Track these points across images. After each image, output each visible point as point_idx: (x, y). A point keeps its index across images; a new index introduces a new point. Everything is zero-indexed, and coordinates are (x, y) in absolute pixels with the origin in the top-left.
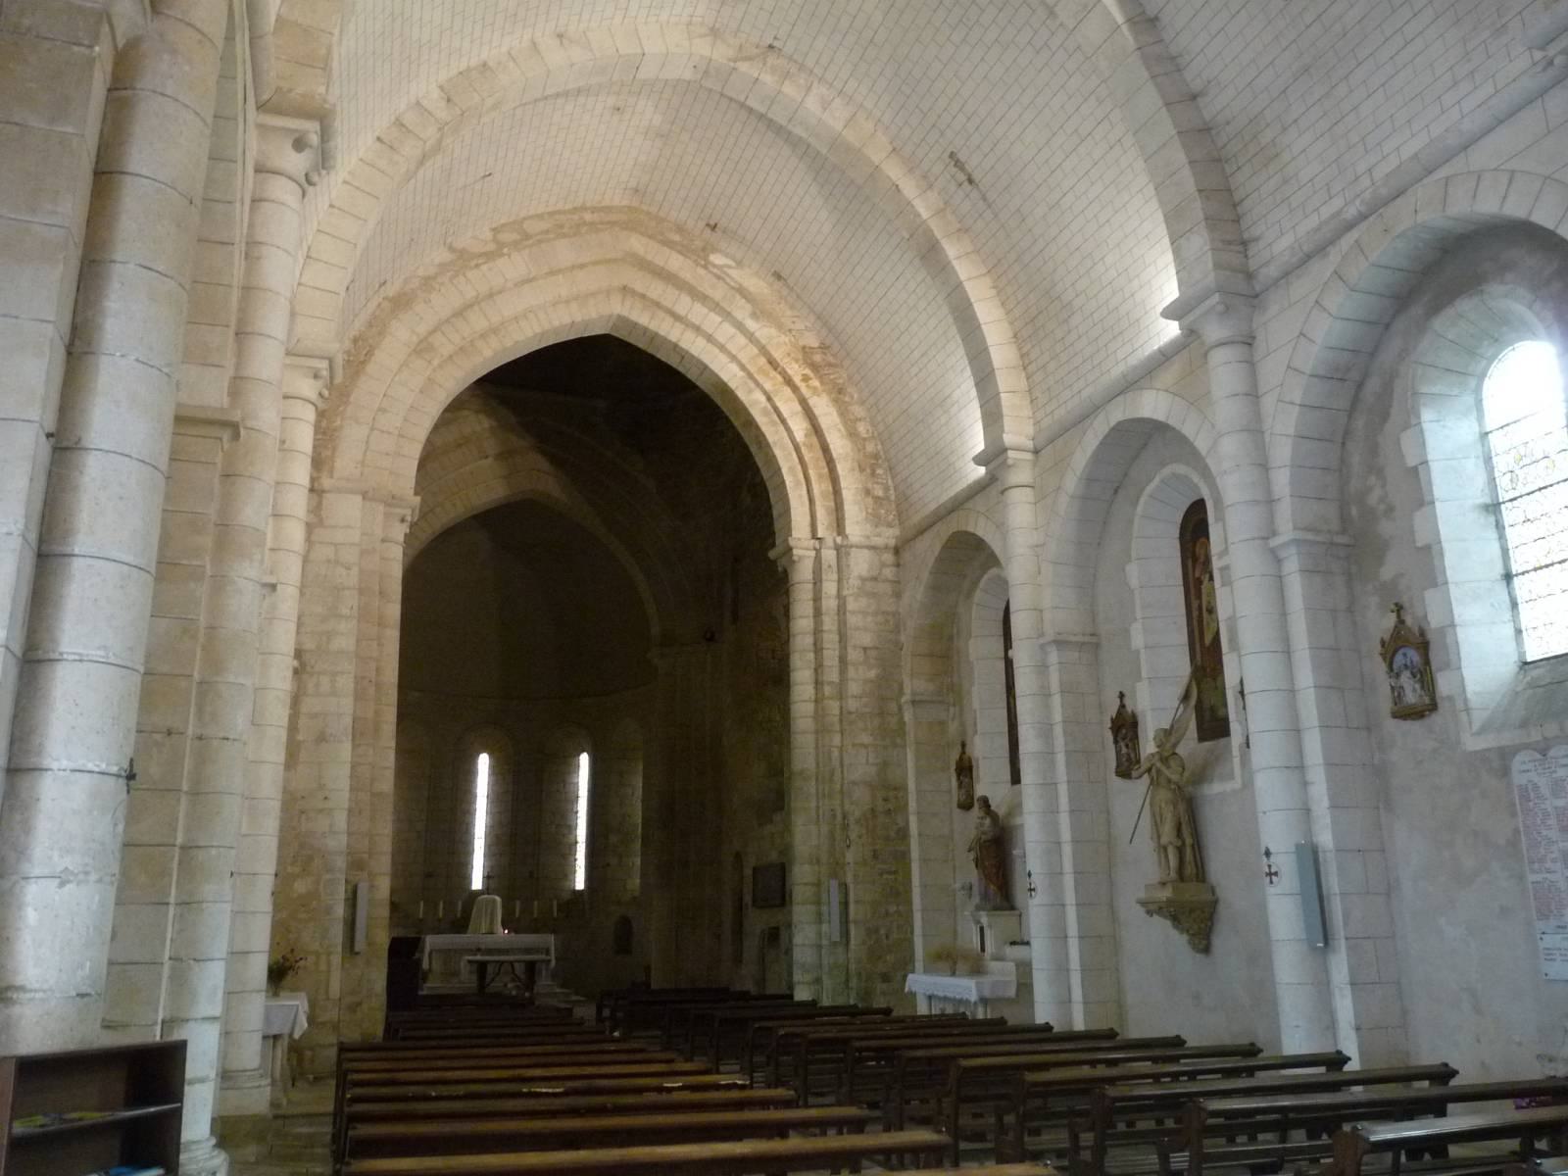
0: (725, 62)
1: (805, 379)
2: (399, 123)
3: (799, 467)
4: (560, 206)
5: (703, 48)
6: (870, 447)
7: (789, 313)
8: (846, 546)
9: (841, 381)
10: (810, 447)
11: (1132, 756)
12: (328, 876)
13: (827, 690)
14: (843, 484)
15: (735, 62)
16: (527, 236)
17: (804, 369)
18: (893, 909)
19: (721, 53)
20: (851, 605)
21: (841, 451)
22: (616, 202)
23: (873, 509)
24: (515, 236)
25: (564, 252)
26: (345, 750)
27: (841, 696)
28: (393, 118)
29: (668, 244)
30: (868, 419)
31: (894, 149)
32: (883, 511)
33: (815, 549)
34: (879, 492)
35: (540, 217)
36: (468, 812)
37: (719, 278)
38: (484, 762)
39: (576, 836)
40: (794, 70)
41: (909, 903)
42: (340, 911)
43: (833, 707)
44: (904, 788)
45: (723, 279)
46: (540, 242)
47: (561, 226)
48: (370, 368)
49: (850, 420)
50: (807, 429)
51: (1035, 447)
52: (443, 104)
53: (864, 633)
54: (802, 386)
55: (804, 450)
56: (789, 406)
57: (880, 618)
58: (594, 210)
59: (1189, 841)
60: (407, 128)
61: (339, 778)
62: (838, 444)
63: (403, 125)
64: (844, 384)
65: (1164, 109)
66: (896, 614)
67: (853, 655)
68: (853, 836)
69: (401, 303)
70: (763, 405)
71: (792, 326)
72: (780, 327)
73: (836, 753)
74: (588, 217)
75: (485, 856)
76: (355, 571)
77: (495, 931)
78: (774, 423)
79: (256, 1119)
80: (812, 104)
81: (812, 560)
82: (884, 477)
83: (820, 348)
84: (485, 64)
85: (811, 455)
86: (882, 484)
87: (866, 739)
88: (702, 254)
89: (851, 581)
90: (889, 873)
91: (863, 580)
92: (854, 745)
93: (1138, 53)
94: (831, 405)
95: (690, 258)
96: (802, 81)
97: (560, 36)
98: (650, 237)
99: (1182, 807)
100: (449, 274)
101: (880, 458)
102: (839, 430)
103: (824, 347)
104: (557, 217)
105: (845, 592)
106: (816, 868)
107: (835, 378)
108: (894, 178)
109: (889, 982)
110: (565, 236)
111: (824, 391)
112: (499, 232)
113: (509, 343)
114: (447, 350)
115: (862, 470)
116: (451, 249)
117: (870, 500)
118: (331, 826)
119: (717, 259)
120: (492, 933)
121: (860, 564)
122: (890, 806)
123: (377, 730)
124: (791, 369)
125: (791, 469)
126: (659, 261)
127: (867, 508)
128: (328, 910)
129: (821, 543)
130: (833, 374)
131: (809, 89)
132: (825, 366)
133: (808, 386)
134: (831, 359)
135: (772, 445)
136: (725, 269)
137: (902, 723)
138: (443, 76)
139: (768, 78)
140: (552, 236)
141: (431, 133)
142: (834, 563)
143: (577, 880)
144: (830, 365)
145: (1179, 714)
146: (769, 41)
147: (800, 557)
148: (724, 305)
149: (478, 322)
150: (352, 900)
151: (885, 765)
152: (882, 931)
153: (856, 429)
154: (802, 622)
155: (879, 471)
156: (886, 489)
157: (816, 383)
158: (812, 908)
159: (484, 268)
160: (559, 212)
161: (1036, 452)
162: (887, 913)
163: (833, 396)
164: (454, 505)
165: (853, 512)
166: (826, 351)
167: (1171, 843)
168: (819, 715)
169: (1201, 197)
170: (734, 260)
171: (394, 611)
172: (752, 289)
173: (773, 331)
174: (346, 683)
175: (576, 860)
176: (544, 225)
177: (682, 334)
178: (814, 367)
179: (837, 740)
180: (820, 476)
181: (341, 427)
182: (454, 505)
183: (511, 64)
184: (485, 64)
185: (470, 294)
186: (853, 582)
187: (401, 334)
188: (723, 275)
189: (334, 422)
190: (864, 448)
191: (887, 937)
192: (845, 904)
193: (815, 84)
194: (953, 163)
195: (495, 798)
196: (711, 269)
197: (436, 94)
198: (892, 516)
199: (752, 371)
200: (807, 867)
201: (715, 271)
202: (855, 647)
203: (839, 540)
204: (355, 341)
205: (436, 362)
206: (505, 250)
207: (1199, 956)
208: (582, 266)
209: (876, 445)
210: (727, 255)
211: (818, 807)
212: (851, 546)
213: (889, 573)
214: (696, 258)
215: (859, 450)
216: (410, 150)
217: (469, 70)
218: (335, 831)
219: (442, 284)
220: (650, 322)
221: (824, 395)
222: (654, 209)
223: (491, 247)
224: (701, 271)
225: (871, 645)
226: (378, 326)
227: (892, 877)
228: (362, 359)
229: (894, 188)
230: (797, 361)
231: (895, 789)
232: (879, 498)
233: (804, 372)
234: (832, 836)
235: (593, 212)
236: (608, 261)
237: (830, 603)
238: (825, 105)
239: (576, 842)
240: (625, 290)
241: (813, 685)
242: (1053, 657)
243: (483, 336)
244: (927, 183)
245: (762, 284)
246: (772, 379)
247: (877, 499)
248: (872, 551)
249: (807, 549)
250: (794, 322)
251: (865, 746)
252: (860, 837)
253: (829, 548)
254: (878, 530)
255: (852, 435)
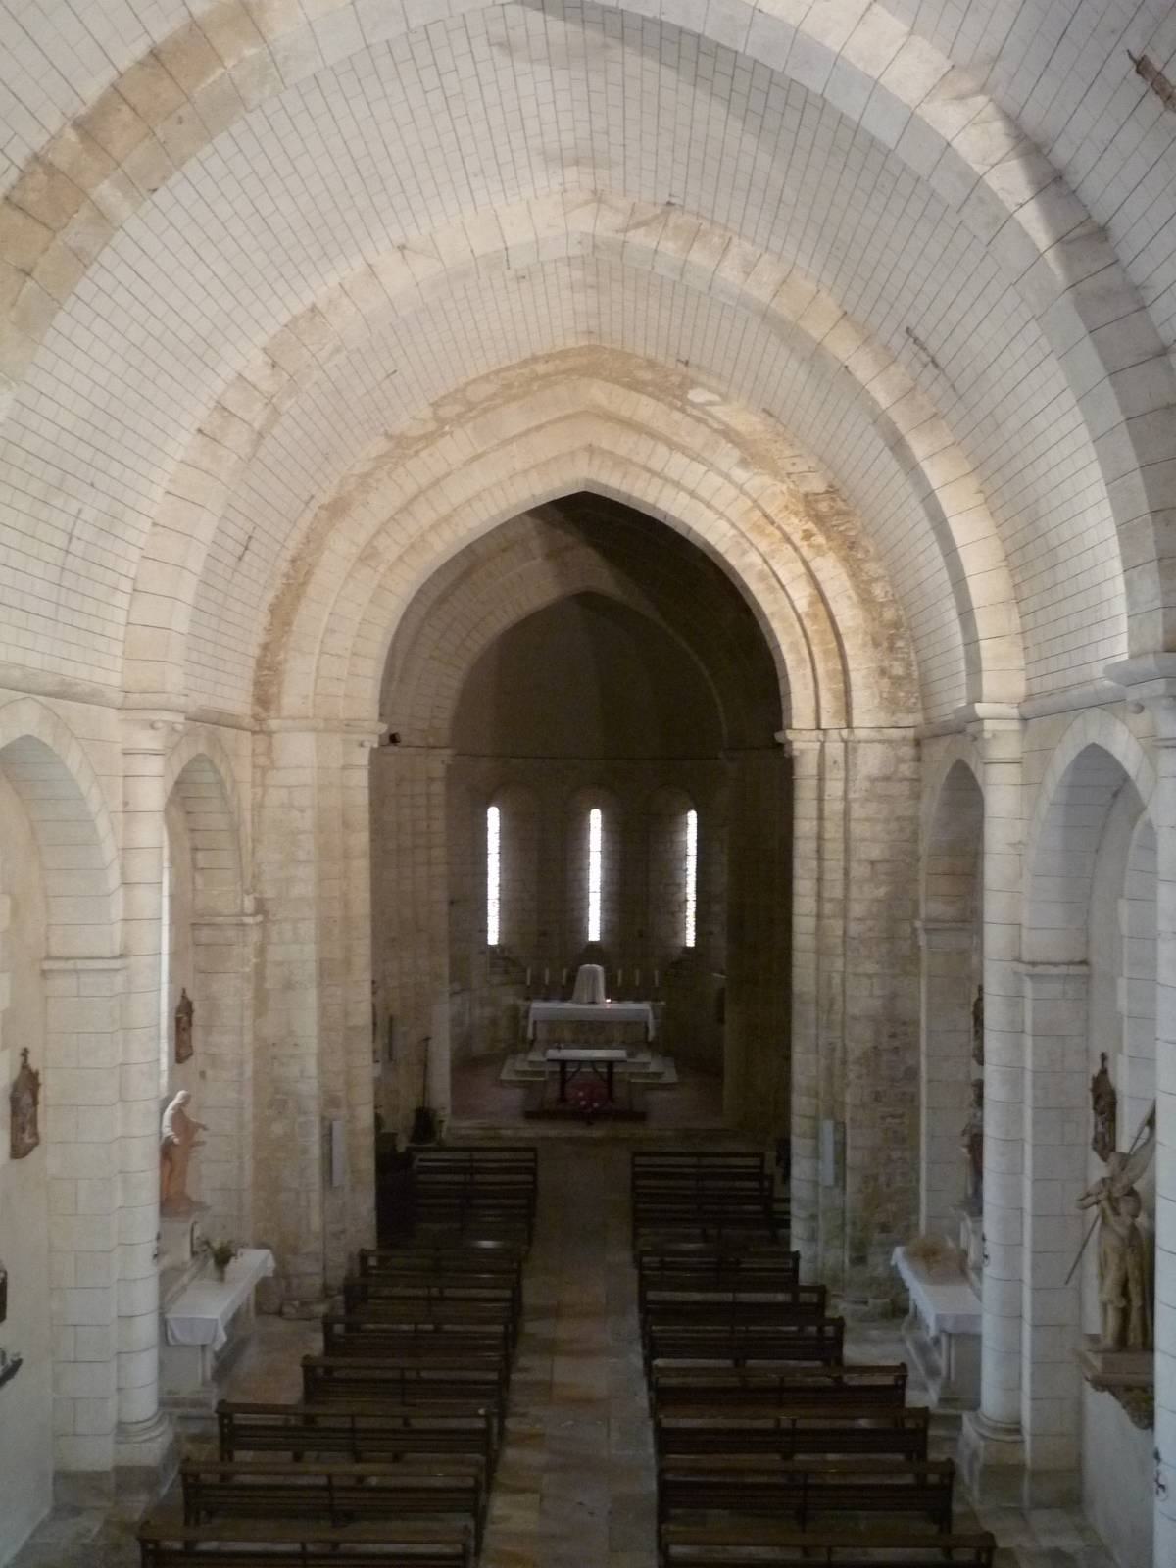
0: (611, 234)
1: (807, 536)
2: (221, 407)
3: (803, 640)
4: (506, 363)
5: (584, 222)
6: (889, 614)
7: (788, 452)
8: (853, 741)
9: (852, 533)
10: (815, 617)
11: (1108, 1139)
12: (301, 1119)
13: (828, 907)
14: (851, 665)
15: (626, 231)
16: (471, 406)
17: (806, 523)
18: (896, 1155)
19: (606, 225)
20: (857, 811)
21: (850, 624)
22: (571, 343)
23: (889, 692)
24: (458, 408)
25: (513, 419)
26: (311, 997)
27: (845, 914)
28: (212, 404)
29: (636, 386)
30: (887, 579)
31: (845, 313)
32: (902, 694)
33: (819, 741)
34: (898, 670)
35: (486, 378)
36: (582, 869)
37: (699, 420)
38: (596, 817)
39: (686, 893)
40: (706, 225)
41: (916, 1147)
42: (315, 1151)
43: (836, 926)
44: (917, 1023)
45: (705, 422)
46: (486, 410)
47: (509, 386)
48: (311, 590)
49: (863, 581)
50: (811, 595)
51: (1021, 716)
52: (268, 372)
53: (872, 841)
54: (803, 546)
55: (807, 623)
56: (788, 570)
57: (894, 826)
58: (548, 358)
59: (1136, 1302)
60: (230, 412)
61: (307, 1024)
62: (848, 615)
63: (225, 409)
64: (857, 535)
65: (1107, 382)
66: (914, 820)
67: (858, 871)
68: (851, 1076)
69: (338, 509)
70: (760, 568)
71: (791, 470)
72: (776, 473)
73: (837, 980)
74: (541, 368)
75: (601, 910)
76: (309, 814)
77: (597, 1000)
78: (771, 589)
79: (149, 1471)
80: (730, 273)
81: (817, 752)
82: (906, 650)
83: (827, 492)
84: (313, 308)
85: (815, 627)
86: (903, 659)
87: (870, 967)
88: (678, 392)
89: (857, 782)
90: (893, 1116)
91: (873, 780)
92: (855, 975)
93: (1069, 295)
94: (838, 565)
95: (662, 400)
96: (716, 240)
97: (402, 248)
98: (616, 381)
99: (1130, 1260)
100: (386, 468)
101: (902, 626)
102: (849, 597)
103: (832, 491)
104: (502, 375)
105: (851, 795)
106: (814, 1101)
107: (846, 530)
108: (842, 356)
109: (888, 1232)
110: (515, 398)
111: (830, 548)
112: (439, 406)
113: (462, 532)
114: (391, 555)
115: (876, 644)
116: (388, 436)
117: (885, 682)
118: (302, 1072)
119: (697, 396)
120: (593, 1002)
121: (871, 761)
122: (896, 1043)
123: (347, 963)
124: (789, 525)
125: (794, 645)
126: (625, 412)
127: (881, 692)
128: (304, 1151)
129: (825, 735)
130: (842, 524)
131: (726, 249)
132: (834, 515)
133: (810, 546)
134: (840, 505)
135: (769, 617)
136: (708, 408)
137: (916, 947)
138: (261, 339)
139: (670, 247)
140: (499, 401)
141: (257, 415)
142: (841, 760)
143: (688, 936)
144: (839, 513)
145: (1136, 1147)
146: (667, 198)
147: (802, 752)
148: (706, 454)
149: (425, 515)
150: (328, 1136)
151: (893, 997)
152: (882, 1179)
153: (870, 592)
154: (804, 826)
155: (900, 644)
156: (909, 665)
157: (820, 539)
158: (810, 1142)
159: (424, 454)
160: (508, 369)
161: (1024, 720)
162: (889, 1160)
163: (843, 553)
164: (505, 612)
165: (863, 699)
166: (834, 496)
167: (1112, 1302)
168: (819, 932)
169: (1154, 523)
170: (721, 395)
171: (361, 839)
172: (741, 428)
173: (767, 480)
174: (308, 929)
175: (686, 917)
176: (488, 389)
177: (661, 491)
178: (819, 519)
179: (839, 964)
180: (826, 652)
181: (286, 660)
182: (505, 612)
183: (345, 301)
184: (313, 308)
185: (411, 488)
186: (860, 785)
187: (342, 545)
188: (705, 417)
189: (278, 655)
190: (881, 616)
191: (888, 1185)
192: (841, 1147)
193: (735, 240)
194: (912, 340)
195: (608, 855)
196: (689, 409)
197: (260, 358)
198: (913, 700)
199: (743, 530)
200: (804, 1099)
201: (695, 412)
202: (860, 862)
203: (845, 733)
204: (293, 561)
205: (382, 569)
206: (447, 428)
207: (1144, 1432)
208: (539, 428)
209: (897, 609)
210: (710, 389)
211: (817, 1037)
212: (860, 742)
213: (906, 770)
214: (671, 398)
215: (874, 620)
216: (238, 438)
217: (295, 319)
218: (306, 1075)
219: (379, 481)
220: (622, 483)
221: (831, 553)
222: (618, 346)
223: (432, 426)
224: (677, 415)
225: (880, 859)
226: (314, 541)
227: (897, 1121)
228: (301, 580)
229: (843, 369)
230: (796, 514)
231: (904, 1023)
232: (899, 678)
233: (805, 527)
234: (829, 1070)
235: (547, 361)
236: (568, 417)
237: (834, 807)
238: (748, 268)
239: (686, 900)
240: (591, 449)
241: (814, 898)
242: (1028, 988)
243: (434, 527)
244: (888, 358)
245: (754, 419)
246: (768, 535)
247: (896, 681)
248: (886, 745)
249: (810, 741)
250: (794, 464)
251: (870, 976)
252: (860, 1077)
253: (836, 741)
254: (894, 719)
255: (866, 600)
